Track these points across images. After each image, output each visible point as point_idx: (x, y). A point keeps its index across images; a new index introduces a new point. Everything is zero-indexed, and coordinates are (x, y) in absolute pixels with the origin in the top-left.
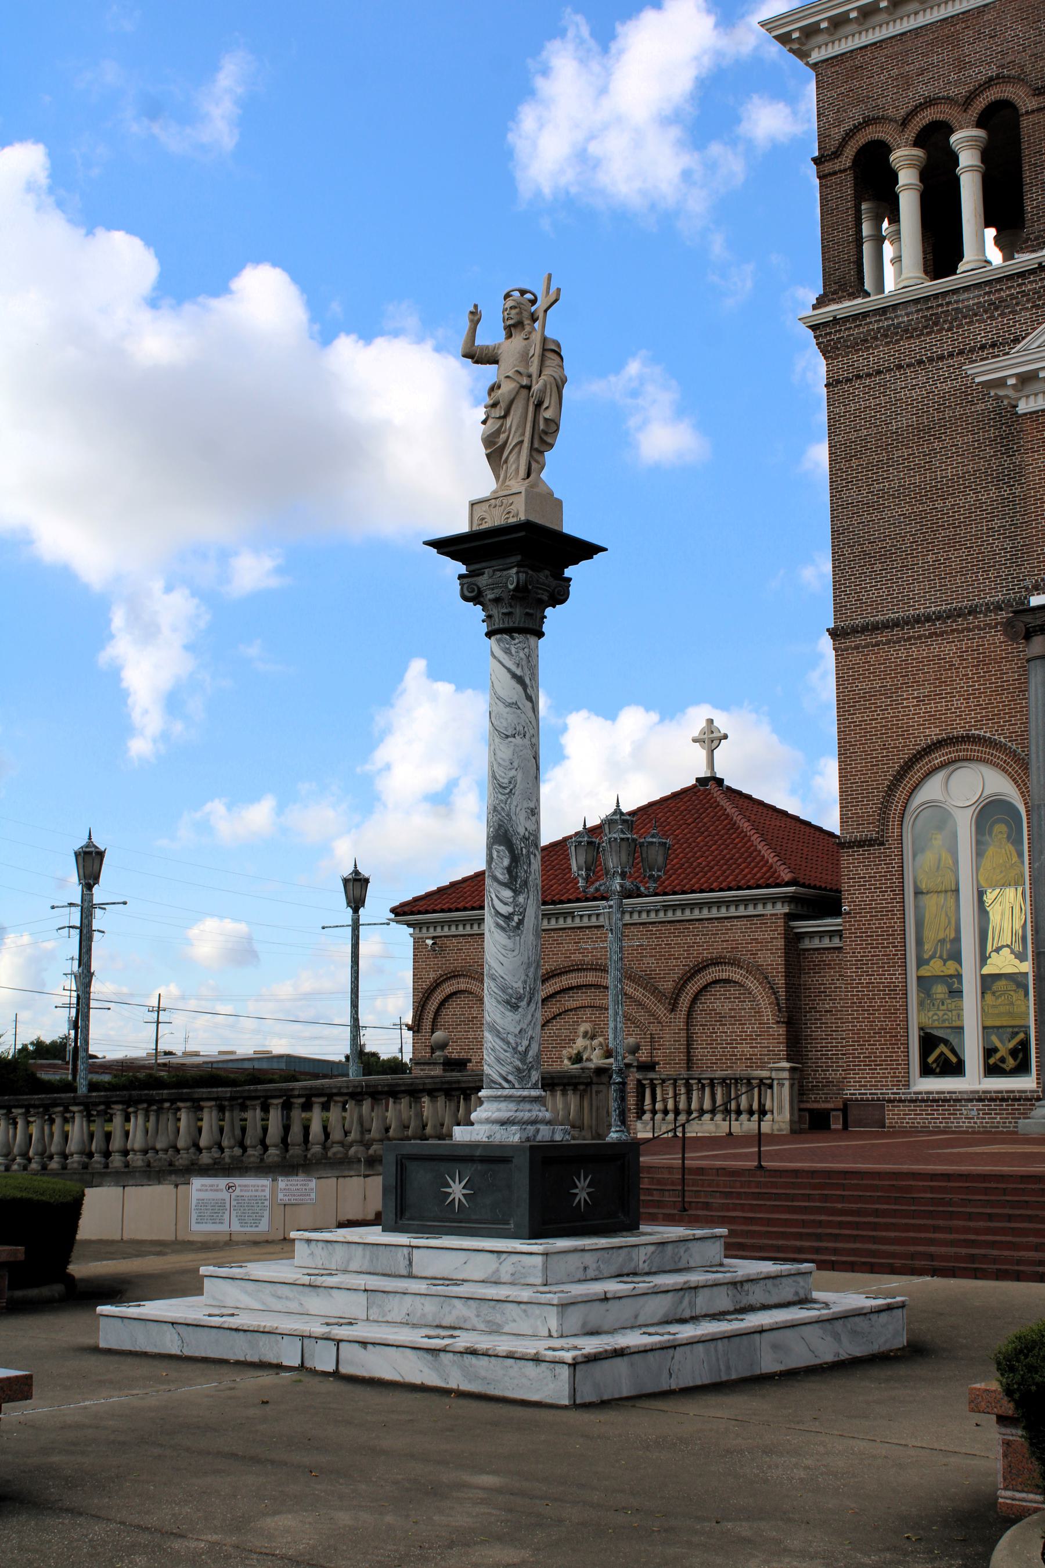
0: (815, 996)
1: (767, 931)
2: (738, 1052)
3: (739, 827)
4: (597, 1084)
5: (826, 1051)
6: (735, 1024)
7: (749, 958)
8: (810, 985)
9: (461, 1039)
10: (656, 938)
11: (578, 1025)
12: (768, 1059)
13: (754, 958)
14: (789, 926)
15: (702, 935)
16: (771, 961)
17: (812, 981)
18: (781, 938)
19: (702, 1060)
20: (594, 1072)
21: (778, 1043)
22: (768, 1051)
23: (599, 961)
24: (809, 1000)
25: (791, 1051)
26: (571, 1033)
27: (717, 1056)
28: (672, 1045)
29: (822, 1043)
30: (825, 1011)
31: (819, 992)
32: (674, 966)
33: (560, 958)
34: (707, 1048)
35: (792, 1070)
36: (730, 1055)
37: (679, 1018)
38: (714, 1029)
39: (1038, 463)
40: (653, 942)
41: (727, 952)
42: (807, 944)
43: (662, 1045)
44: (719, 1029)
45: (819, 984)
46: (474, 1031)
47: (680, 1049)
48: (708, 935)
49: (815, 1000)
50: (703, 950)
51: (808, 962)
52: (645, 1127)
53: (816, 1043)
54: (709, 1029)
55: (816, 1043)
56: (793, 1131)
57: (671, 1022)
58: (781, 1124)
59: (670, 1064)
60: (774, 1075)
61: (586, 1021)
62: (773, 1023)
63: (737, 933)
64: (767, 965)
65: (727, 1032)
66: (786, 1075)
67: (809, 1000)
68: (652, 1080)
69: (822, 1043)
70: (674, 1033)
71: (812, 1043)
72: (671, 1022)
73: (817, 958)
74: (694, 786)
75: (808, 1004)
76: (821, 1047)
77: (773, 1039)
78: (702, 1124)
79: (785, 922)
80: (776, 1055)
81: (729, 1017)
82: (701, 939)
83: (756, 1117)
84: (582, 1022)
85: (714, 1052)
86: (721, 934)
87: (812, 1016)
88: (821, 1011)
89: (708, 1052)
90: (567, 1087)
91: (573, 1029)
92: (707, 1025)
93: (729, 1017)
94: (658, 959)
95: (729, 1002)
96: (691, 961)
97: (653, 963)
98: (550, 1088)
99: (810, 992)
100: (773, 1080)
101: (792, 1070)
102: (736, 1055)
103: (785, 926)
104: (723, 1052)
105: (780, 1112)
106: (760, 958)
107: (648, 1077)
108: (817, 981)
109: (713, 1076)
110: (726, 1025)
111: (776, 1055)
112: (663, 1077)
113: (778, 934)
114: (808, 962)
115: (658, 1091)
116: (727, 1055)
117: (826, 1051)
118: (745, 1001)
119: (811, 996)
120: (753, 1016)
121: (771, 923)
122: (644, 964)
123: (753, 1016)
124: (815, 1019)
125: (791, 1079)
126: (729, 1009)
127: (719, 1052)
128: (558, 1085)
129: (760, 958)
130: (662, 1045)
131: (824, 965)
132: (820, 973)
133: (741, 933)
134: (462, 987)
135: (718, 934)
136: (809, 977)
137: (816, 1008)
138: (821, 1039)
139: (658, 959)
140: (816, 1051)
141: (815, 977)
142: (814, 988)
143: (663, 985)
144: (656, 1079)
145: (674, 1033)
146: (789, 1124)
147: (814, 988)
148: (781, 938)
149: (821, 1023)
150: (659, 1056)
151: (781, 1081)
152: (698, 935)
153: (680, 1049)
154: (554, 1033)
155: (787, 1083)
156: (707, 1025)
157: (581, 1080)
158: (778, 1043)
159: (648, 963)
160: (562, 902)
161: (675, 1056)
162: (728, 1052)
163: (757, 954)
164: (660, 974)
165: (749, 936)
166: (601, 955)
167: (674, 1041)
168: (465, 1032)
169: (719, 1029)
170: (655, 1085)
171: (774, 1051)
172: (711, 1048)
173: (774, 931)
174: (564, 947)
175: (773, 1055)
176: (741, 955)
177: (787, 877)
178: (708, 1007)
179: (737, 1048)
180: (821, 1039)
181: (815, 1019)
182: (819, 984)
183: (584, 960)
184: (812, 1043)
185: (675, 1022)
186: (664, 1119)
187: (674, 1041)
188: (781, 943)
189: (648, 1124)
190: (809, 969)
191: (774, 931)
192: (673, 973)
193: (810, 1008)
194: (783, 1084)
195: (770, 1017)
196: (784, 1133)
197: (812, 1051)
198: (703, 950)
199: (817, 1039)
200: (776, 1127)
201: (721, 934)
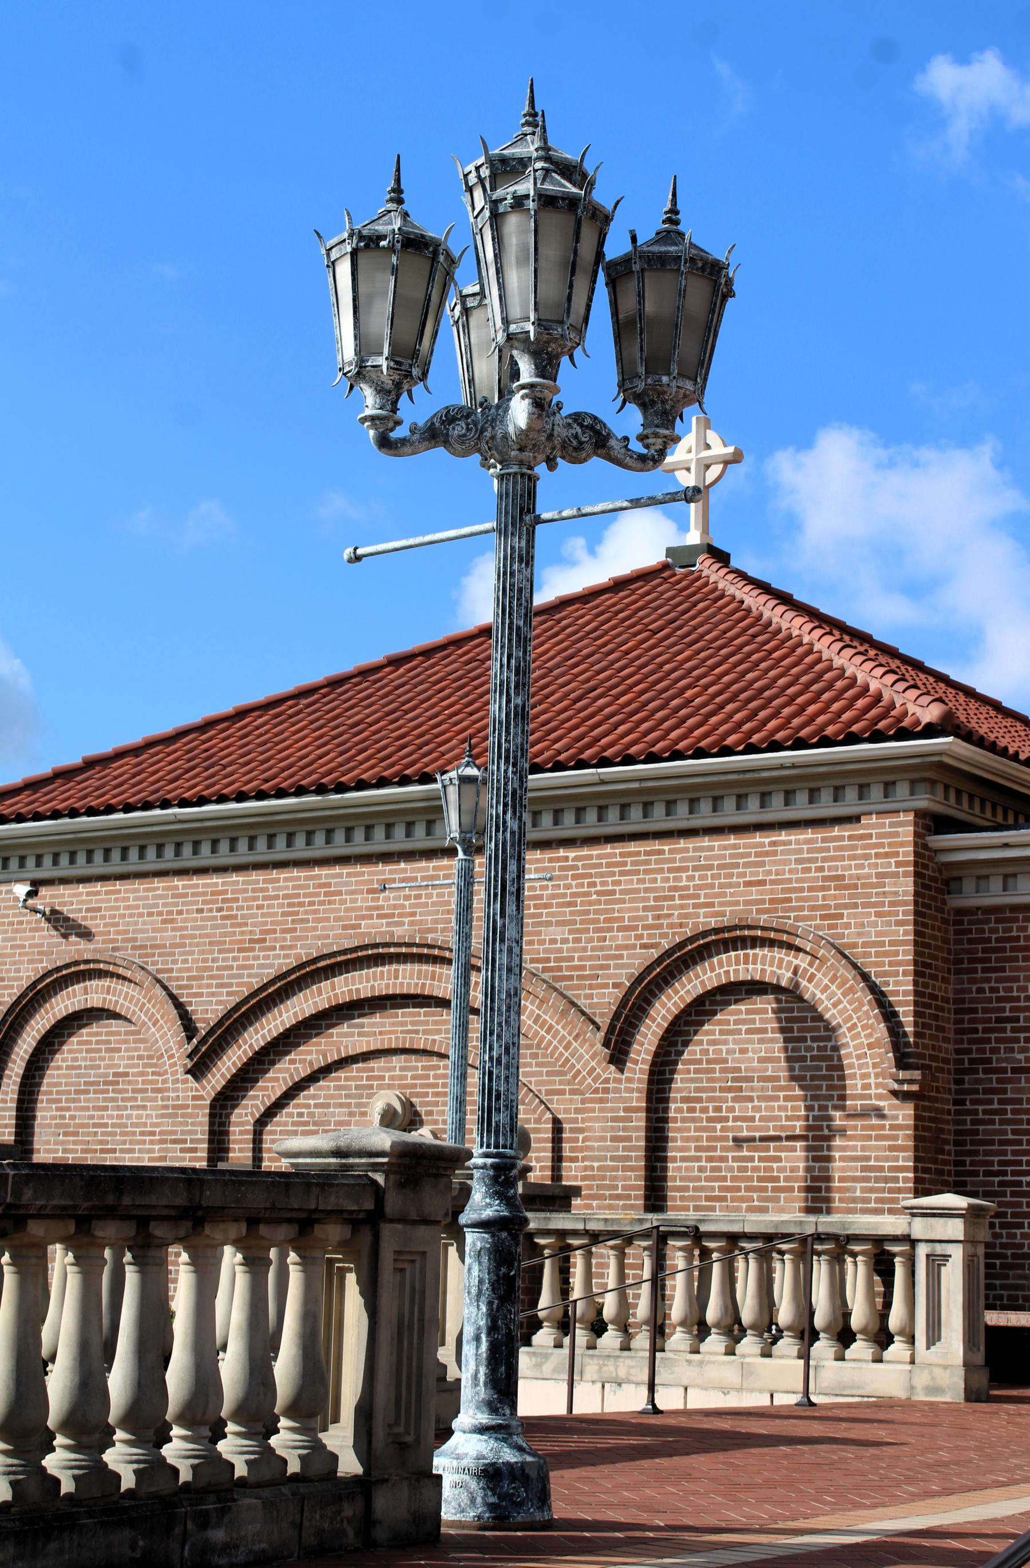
0: (986, 1030)
1: (867, 857)
2: (781, 1170)
3: (779, 631)
4: (403, 1220)
5: (1014, 1173)
6: (776, 1098)
7: (818, 927)
8: (972, 1001)
9: (87, 1126)
10: (574, 877)
11: (370, 1096)
12: (863, 1190)
13: (831, 927)
14: (925, 847)
15: (695, 869)
16: (878, 934)
17: (981, 990)
18: (906, 874)
19: (686, 1189)
20: (387, 1170)
21: (891, 1148)
22: (864, 1169)
23: (430, 936)
24: (971, 1041)
25: (925, 1170)
26: (351, 1114)
27: (724, 1179)
28: (607, 1149)
29: (1004, 1153)
30: (1015, 1070)
31: (998, 1020)
32: (618, 947)
33: (333, 928)
34: (698, 1159)
35: (972, 1215)
36: (760, 1179)
37: (630, 1080)
38: (718, 1109)
39: (731, 876)
40: (568, 887)
41: (759, 911)
42: (970, 897)
43: (582, 1149)
44: (731, 1109)
45: (999, 999)
46: (118, 1108)
47: (628, 1158)
48: (710, 867)
49: (988, 1041)
50: (696, 906)
51: (971, 941)
52: (538, 1366)
53: (987, 1153)
54: (705, 1110)
55: (987, 1153)
56: (972, 1395)
57: (606, 1090)
58: (938, 1371)
59: (603, 1197)
60: (919, 1228)
61: (390, 1087)
62: (879, 1097)
63: (788, 862)
64: (865, 945)
65: (752, 1119)
66: (955, 1228)
67: (971, 1041)
68: (562, 1234)
69: (1004, 1153)
70: (614, 1119)
71: (976, 1153)
72: (606, 1090)
73: (993, 931)
74: (665, 567)
75: (969, 1051)
76: (1001, 1163)
77: (879, 1138)
78: (701, 1363)
79: (916, 834)
80: (886, 1180)
81: (762, 1079)
82: (691, 878)
83: (787, 1345)
84: (380, 1087)
85: (719, 1169)
86: (746, 865)
87: (978, 1081)
88: (1004, 1070)
89: (701, 1169)
90: (263, 1230)
91: (358, 1105)
92: (699, 1100)
93: (762, 1079)
94: (578, 931)
95: (761, 1041)
96: (664, 936)
97: (565, 941)
98: (183, 1230)
99: (972, 1021)
100: (913, 1242)
101: (972, 1215)
102: (776, 1179)
103: (916, 844)
104: (741, 1169)
105: (934, 1336)
106: (848, 926)
107: (552, 1226)
108: (993, 990)
109: (736, 1228)
110: (751, 1099)
111: (886, 1180)
112: (592, 1226)
113: (898, 864)
114: (971, 941)
115: (578, 1260)
116: (750, 1179)
117: (1014, 1173)
118: (804, 1039)
119: (975, 1031)
120: (824, 1078)
121: (879, 836)
122: (542, 942)
123: (824, 1078)
124: (986, 1091)
125: (969, 1241)
126: (761, 1060)
127: (731, 1169)
128: (218, 1214)
129: (848, 926)
130: (582, 1149)
131: (1013, 949)
132: (1003, 969)
133: (798, 861)
134: (95, 1000)
135: (736, 866)
136: (974, 981)
137: (989, 1061)
138: (1002, 1143)
139: (578, 931)
140: (987, 1173)
141: (988, 980)
142: (985, 1010)
143: (590, 996)
144: (575, 1233)
145: (614, 1119)
146: (961, 1372)
147: (985, 1010)
148: (906, 874)
149: (1001, 1102)
150: (572, 1174)
151: (939, 1249)
152: (685, 869)
153: (628, 1158)
154: (311, 1115)
155: (957, 1253)
156: (699, 1100)
157: (332, 1202)
158: (891, 1148)
159: (553, 941)
160: (341, 788)
161: (613, 1178)
162: (756, 1169)
163: (841, 916)
164: (583, 968)
165: (821, 869)
166: (436, 921)
167: (614, 1139)
168: (96, 1108)
169: (731, 1109)
170: (571, 1248)
171: (881, 1169)
172: (710, 1159)
173: (887, 855)
174: (343, 902)
175: (877, 1180)
176: (797, 919)
177: (930, 714)
178: (706, 1052)
179: (778, 1159)
180: (1002, 1143)
181: (986, 1091)
182: (999, 999)
183: (392, 934)
184: (976, 1153)
185: (617, 1090)
186: (591, 1346)
187: (614, 1139)
188: (906, 887)
189: (546, 1356)
190: (971, 961)
191: (887, 855)
192: (617, 967)
193: (972, 1061)
194: (946, 1257)
195: (872, 1081)
196: (947, 1399)
197: (976, 1174)
198: (696, 906)
199: (992, 1142)
200: (922, 1379)
201: (746, 865)
